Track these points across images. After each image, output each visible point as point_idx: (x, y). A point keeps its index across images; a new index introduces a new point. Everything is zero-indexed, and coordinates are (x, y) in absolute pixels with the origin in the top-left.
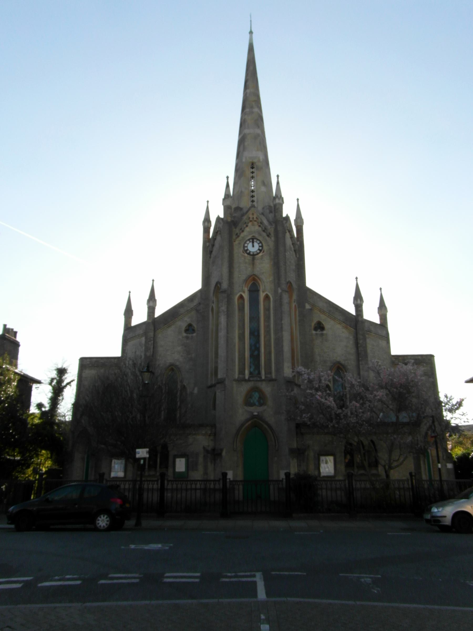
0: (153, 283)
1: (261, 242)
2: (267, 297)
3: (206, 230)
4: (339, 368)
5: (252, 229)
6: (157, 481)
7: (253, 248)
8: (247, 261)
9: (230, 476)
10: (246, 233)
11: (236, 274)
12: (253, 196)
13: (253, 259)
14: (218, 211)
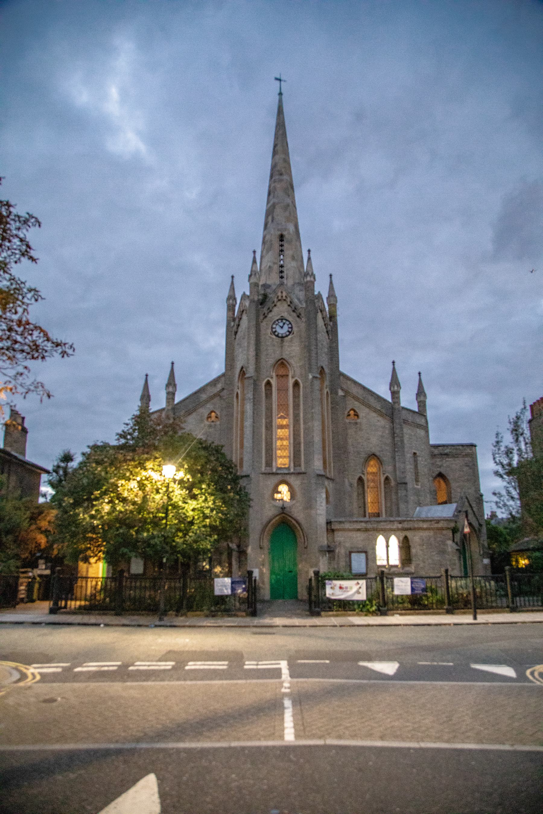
1: (290, 323)
2: (296, 384)
11: (263, 357)
13: (282, 341)
14: (243, 288)
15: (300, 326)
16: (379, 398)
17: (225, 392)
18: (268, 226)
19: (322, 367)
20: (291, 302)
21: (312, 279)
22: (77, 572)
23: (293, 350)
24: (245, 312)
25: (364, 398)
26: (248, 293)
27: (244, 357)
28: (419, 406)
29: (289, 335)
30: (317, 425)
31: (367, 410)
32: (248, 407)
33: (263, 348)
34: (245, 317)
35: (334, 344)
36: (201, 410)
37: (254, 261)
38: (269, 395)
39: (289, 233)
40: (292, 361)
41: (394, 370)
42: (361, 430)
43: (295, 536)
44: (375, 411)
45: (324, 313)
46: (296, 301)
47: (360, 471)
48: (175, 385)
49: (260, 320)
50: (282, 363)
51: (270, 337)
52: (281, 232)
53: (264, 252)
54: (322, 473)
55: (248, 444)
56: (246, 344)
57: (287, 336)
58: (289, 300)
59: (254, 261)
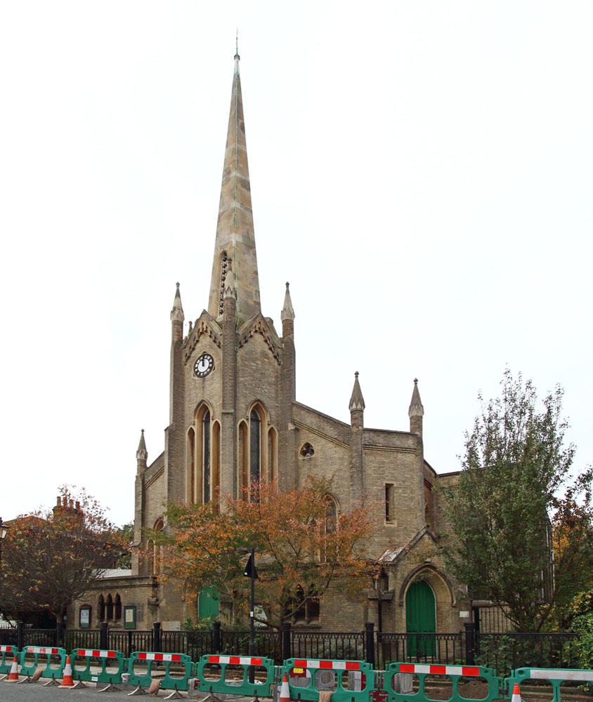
0: (143, 434)
1: (212, 358)
2: (271, 432)
3: (178, 325)
8: (197, 385)
13: (204, 381)
20: (211, 332)
25: (319, 427)
28: (352, 419)
29: (210, 371)
31: (323, 441)
40: (212, 401)
44: (332, 440)
49: (183, 364)
51: (193, 379)
52: (235, 257)
57: (208, 374)
58: (209, 331)
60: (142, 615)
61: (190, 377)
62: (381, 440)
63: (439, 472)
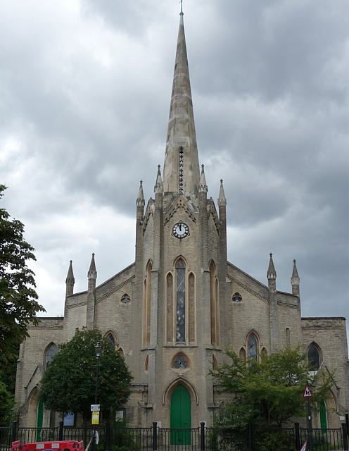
0: (93, 257)
2: (191, 275)
4: (253, 335)
5: (179, 215)
6: (151, 428)
7: (181, 232)
9: (159, 425)
10: (176, 218)
11: (166, 255)
12: (181, 180)
13: (181, 241)
14: (150, 193)
15: (196, 228)
16: (259, 284)
17: (135, 280)
18: (170, 138)
19: (213, 261)
21: (205, 191)
22: (124, 402)
23: (190, 249)
24: (151, 215)
26: (154, 198)
27: (151, 252)
30: (197, 441)
32: (154, 295)
33: (166, 247)
34: (151, 219)
35: (223, 240)
36: (117, 293)
37: (159, 173)
38: (170, 285)
39: (187, 146)
41: (271, 260)
42: (244, 310)
43: (190, 396)
45: (215, 215)
46: (192, 208)
47: (242, 343)
48: (96, 273)
50: (180, 260)
53: (167, 161)
54: (211, 347)
55: (154, 323)
56: (152, 242)
57: (185, 237)
58: (186, 207)
59: (159, 173)
60: (132, 416)
61: (168, 235)
62: (283, 299)
63: (132, 260)
